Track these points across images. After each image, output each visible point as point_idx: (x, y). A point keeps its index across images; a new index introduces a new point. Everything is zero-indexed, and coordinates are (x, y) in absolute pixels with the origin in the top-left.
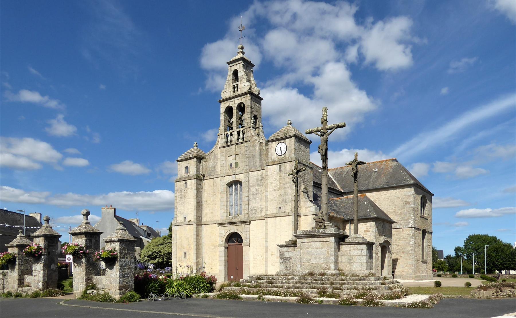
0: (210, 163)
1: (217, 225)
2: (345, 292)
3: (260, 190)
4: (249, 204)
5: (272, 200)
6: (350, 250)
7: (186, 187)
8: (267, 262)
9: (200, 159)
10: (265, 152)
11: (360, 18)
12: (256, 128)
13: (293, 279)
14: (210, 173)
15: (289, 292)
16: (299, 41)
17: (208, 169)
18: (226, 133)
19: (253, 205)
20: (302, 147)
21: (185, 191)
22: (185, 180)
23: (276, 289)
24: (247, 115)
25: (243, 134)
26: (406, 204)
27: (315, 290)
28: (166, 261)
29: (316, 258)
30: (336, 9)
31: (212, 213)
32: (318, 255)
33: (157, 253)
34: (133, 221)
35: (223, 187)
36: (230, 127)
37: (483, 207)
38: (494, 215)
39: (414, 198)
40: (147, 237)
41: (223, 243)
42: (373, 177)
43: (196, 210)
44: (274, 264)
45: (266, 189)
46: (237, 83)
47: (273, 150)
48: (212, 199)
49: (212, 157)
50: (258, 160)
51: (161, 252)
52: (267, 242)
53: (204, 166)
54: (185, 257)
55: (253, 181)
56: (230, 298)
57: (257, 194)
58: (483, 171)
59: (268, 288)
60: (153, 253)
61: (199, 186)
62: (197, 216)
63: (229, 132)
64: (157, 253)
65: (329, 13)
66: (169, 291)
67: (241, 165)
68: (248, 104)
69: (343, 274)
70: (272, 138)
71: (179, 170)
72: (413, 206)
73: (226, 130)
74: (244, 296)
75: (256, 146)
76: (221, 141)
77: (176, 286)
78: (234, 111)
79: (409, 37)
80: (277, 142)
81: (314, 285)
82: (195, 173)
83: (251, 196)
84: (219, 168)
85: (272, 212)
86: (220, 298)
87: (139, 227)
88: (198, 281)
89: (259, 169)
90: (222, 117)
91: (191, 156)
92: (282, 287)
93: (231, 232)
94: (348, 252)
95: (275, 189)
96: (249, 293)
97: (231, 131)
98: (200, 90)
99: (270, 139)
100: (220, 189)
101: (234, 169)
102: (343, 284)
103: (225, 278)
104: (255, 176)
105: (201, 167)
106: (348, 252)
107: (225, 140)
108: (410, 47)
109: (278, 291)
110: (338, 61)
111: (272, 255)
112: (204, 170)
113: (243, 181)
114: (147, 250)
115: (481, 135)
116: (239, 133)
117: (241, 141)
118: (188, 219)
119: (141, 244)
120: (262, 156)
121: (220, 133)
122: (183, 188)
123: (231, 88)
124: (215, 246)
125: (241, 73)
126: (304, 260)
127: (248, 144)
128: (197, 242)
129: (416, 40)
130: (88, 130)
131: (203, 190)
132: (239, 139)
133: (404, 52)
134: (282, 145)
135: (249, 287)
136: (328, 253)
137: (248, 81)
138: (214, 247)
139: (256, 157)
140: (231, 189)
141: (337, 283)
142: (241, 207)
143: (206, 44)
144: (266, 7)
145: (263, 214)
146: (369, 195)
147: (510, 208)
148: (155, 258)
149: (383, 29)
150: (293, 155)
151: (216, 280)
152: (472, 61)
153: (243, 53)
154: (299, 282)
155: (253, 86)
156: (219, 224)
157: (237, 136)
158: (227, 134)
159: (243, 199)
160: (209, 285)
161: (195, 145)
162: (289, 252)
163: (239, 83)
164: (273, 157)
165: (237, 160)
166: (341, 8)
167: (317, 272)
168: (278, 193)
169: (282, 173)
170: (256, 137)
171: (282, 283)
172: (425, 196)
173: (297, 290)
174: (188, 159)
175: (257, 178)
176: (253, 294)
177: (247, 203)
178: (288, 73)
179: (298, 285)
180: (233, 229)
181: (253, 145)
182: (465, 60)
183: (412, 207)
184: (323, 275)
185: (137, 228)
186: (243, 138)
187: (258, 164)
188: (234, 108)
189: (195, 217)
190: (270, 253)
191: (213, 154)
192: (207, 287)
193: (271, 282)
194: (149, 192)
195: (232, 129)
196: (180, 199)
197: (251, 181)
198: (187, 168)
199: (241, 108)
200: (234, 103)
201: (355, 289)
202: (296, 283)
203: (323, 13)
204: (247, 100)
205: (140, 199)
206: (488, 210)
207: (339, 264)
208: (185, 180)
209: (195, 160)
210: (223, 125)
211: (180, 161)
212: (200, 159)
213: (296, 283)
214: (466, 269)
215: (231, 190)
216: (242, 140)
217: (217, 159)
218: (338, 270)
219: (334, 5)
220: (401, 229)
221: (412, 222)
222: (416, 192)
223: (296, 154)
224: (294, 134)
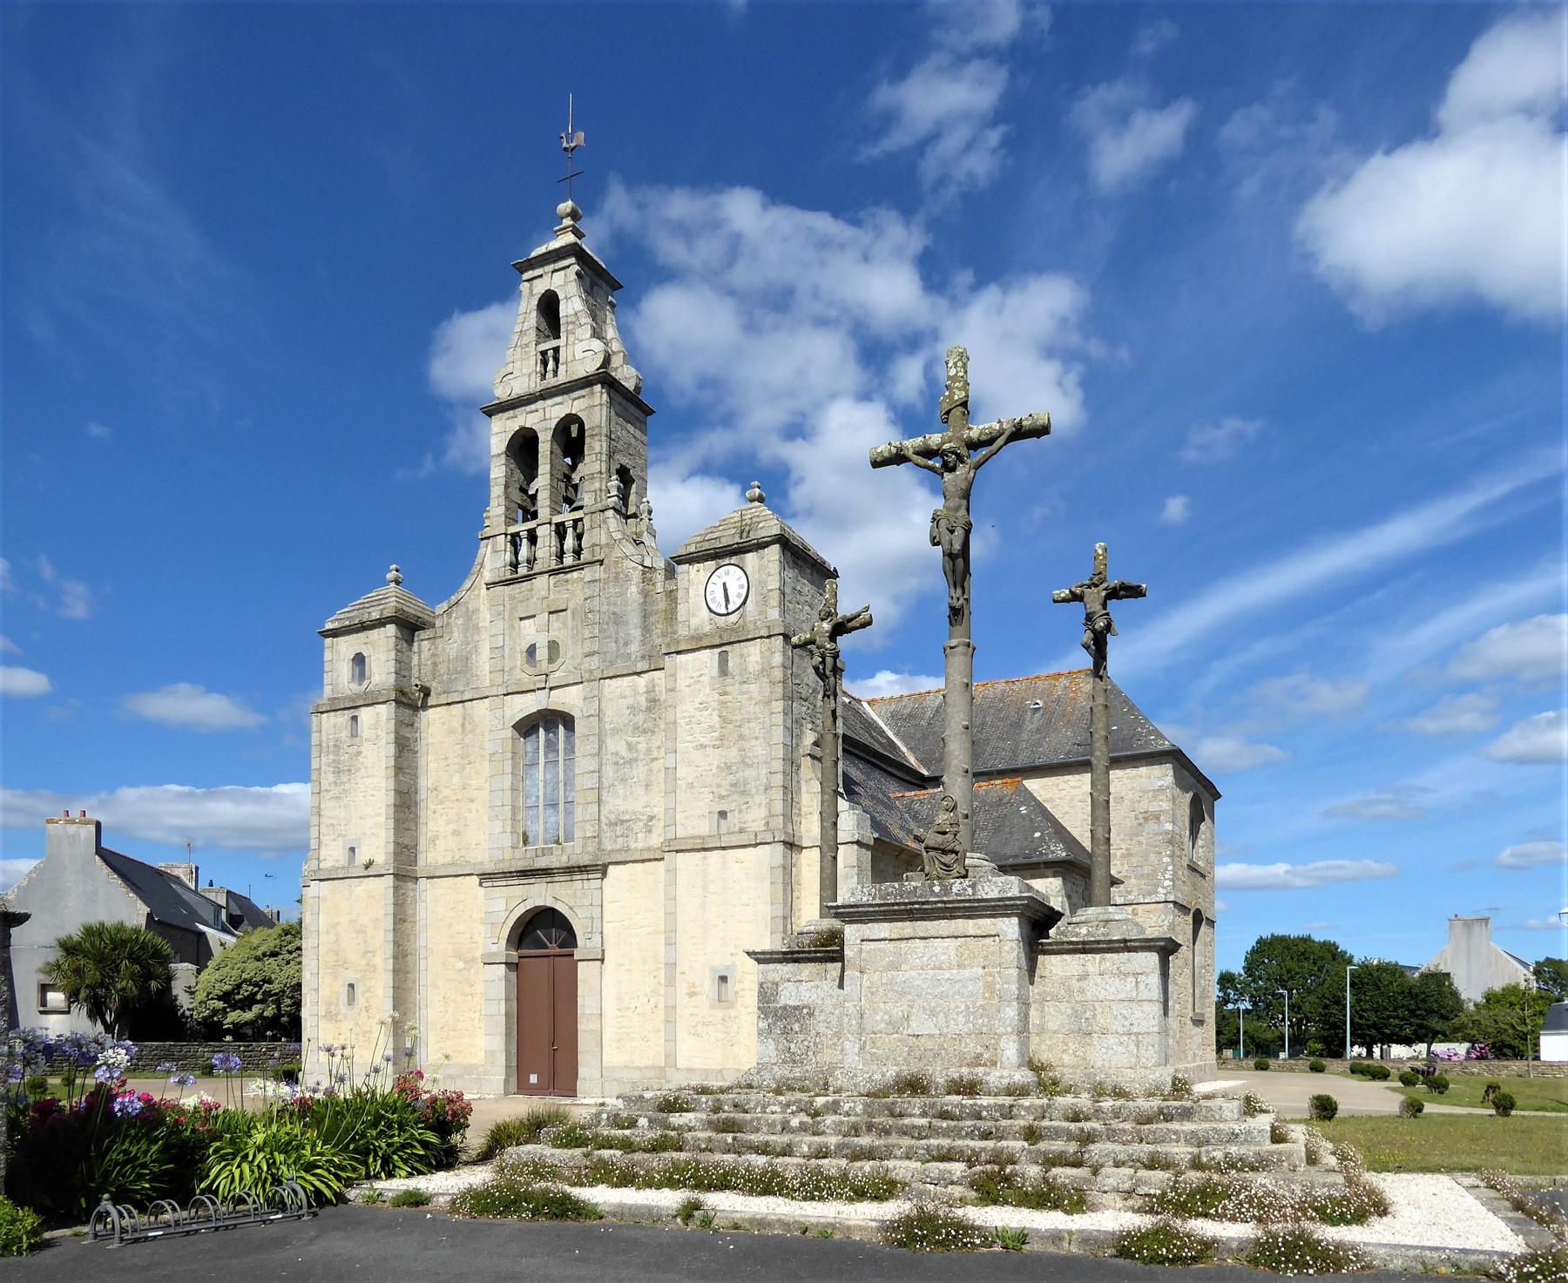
0: (451, 647)
1: (476, 879)
2: (1112, 1182)
3: (642, 747)
4: (599, 802)
5: (691, 785)
6: (1083, 977)
7: (354, 734)
8: (670, 1022)
9: (409, 627)
10: (662, 605)
11: (933, 272)
12: (627, 517)
13: (834, 1108)
14: (451, 681)
15: (828, 1179)
16: (750, 328)
17: (442, 668)
18: (512, 530)
19: (616, 803)
20: (807, 588)
21: (354, 749)
22: (352, 706)
23: (760, 1161)
24: (593, 464)
25: (579, 537)
26: (1146, 819)
27: (958, 1168)
28: (289, 1014)
29: (933, 1014)
30: (864, 236)
31: (456, 833)
32: (942, 996)
33: (256, 985)
34: (176, 872)
36: (525, 511)
37: (1265, 859)
38: (1298, 882)
39: (1174, 800)
40: (224, 930)
41: (500, 948)
42: (1029, 727)
43: (397, 820)
44: (700, 1029)
45: (670, 745)
46: (554, 343)
47: (696, 595)
48: (456, 779)
49: (457, 620)
50: (636, 633)
51: (270, 981)
52: (670, 943)
53: (426, 654)
54: (351, 1000)
55: (615, 712)
56: (535, 1212)
58: (1277, 753)
59: (718, 1157)
60: (239, 986)
61: (406, 732)
62: (397, 844)
63: (522, 528)
64: (256, 985)
65: (842, 246)
66: (227, 1177)
67: (571, 653)
68: (597, 422)
69: (1055, 1083)
72: (1169, 827)
73: (510, 520)
74: (601, 1196)
75: (628, 579)
76: (493, 559)
77: (260, 1149)
78: (545, 448)
79: (1075, 338)
80: (711, 564)
81: (946, 1142)
82: (392, 679)
83: (609, 771)
84: (483, 664)
85: (691, 832)
86: (484, 1211)
87: (196, 892)
88: (378, 1118)
89: (640, 667)
90: (498, 471)
91: (375, 615)
92: (787, 1151)
93: (529, 905)
94: (1075, 985)
95: (704, 741)
96: (626, 1179)
97: (531, 525)
98: (429, 463)
100: (487, 744)
101: (544, 666)
102: (1087, 1139)
103: (506, 1081)
105: (415, 660)
106: (1075, 985)
107: (508, 557)
108: (1078, 368)
109: (775, 1174)
110: (865, 396)
111: (692, 994)
112: (426, 670)
113: (576, 714)
114: (218, 975)
115: (1260, 649)
116: (561, 531)
117: (569, 560)
118: (362, 857)
119: (199, 953)
120: (652, 619)
121: (488, 532)
122: (344, 735)
123: (532, 363)
124: (470, 962)
125: (572, 305)
126: (878, 1020)
127: (596, 572)
128: (396, 944)
129: (1096, 349)
130: (47, 572)
131: (421, 747)
132: (560, 555)
133: (1060, 384)
134: (730, 576)
135: (627, 1146)
136: (989, 987)
137: (597, 334)
139: (627, 623)
141: (1056, 1134)
142: (569, 813)
143: (448, 315)
144: (641, 206)
145: (656, 840)
146: (1033, 785)
147: (1339, 862)
148: (248, 1003)
149: (1000, 310)
150: (774, 614)
151: (466, 1110)
152: (1252, 428)
153: (578, 234)
154: (870, 1127)
155: (617, 361)
156: (486, 877)
157: (554, 541)
158: (515, 536)
159: (578, 781)
160: (432, 1137)
161: (390, 576)
162: (806, 986)
163: (561, 342)
164: (694, 622)
165: (553, 635)
166: (880, 233)
167: (940, 1074)
168: (714, 758)
169: (729, 680)
170: (629, 549)
171: (785, 1127)
172: (1201, 794)
173: (868, 1166)
174: (363, 627)
175: (630, 701)
176: (649, 1184)
177: (593, 796)
178: (711, 425)
179: (865, 1141)
180: (540, 895)
181: (617, 578)
182: (1232, 424)
183: (1167, 833)
184: (969, 1088)
185: (187, 896)
186: (578, 552)
187: (634, 648)
188: (541, 437)
189: (391, 848)
190: (682, 988)
191: (460, 610)
192: (425, 1144)
193: (729, 1126)
194: (257, 789)
195: (534, 516)
196: (331, 778)
197: (609, 713)
198: (359, 660)
199: (571, 439)
200: (543, 419)
201: (1153, 1163)
202: (856, 1130)
203: (824, 244)
204: (592, 408)
205: (226, 809)
206: (1281, 868)
207: (1034, 1039)
208: (352, 706)
209: (391, 629)
210: (502, 501)
211: (335, 633)
212: (409, 627)
213: (856, 1130)
214: (1252, 1038)
215: (529, 749)
217: (477, 629)
218: (1037, 1068)
219: (855, 222)
220: (1130, 908)
221: (1167, 883)
222: (1180, 783)
223: (784, 612)
224: (776, 531)
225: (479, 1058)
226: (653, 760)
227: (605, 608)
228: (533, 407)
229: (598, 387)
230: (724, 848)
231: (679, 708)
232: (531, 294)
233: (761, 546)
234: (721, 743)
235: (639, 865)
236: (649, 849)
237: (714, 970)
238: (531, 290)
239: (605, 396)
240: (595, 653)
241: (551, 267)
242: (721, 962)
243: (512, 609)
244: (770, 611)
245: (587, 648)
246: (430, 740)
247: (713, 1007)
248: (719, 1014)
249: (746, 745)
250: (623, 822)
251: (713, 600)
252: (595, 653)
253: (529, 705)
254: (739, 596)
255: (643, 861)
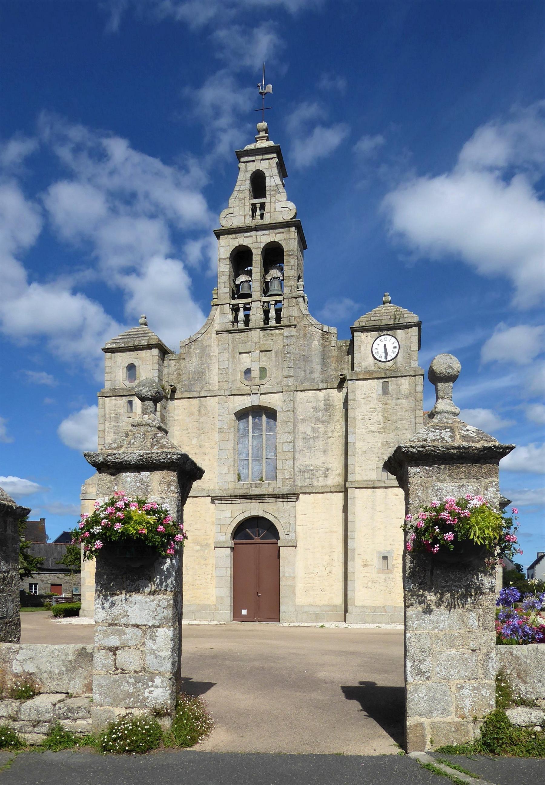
3: (322, 430)
5: (365, 452)
16: (114, 211)
17: (184, 377)
35: (228, 417)
50: (318, 367)
57: (314, 438)
70: (364, 324)
71: (107, 370)
75: (312, 337)
80: (375, 334)
83: (300, 443)
84: (214, 377)
85: (364, 478)
89: (321, 386)
91: (144, 342)
93: (247, 515)
95: (373, 429)
99: (356, 324)
100: (216, 423)
101: (257, 381)
104: (308, 401)
107: (231, 317)
110: (171, 256)
111: (365, 566)
117: (272, 323)
123: (248, 210)
125: (273, 180)
138: (201, 546)
139: (311, 361)
140: (242, 425)
165: (263, 364)
169: (389, 397)
174: (136, 348)
175: (314, 404)
177: (290, 455)
180: (255, 509)
181: (305, 336)
187: (316, 375)
188: (254, 251)
191: (198, 344)
198: (131, 368)
199: (274, 255)
200: (257, 242)
216: (273, 319)
217: (209, 356)
225: (212, 600)
226: (328, 438)
227: (297, 352)
228: (248, 234)
229: (293, 229)
230: (386, 487)
231: (357, 410)
232: (246, 170)
233: (407, 326)
234: (384, 430)
235: (320, 495)
236: (326, 486)
237: (379, 553)
238: (246, 168)
239: (296, 234)
240: (291, 376)
241: (261, 157)
242: (384, 549)
243: (234, 348)
244: (412, 362)
245: (286, 373)
246: (176, 418)
247: (379, 573)
248: (383, 576)
249: (400, 433)
250: (309, 471)
251: (377, 353)
252: (291, 376)
253: (246, 402)
254: (393, 352)
255: (322, 493)
